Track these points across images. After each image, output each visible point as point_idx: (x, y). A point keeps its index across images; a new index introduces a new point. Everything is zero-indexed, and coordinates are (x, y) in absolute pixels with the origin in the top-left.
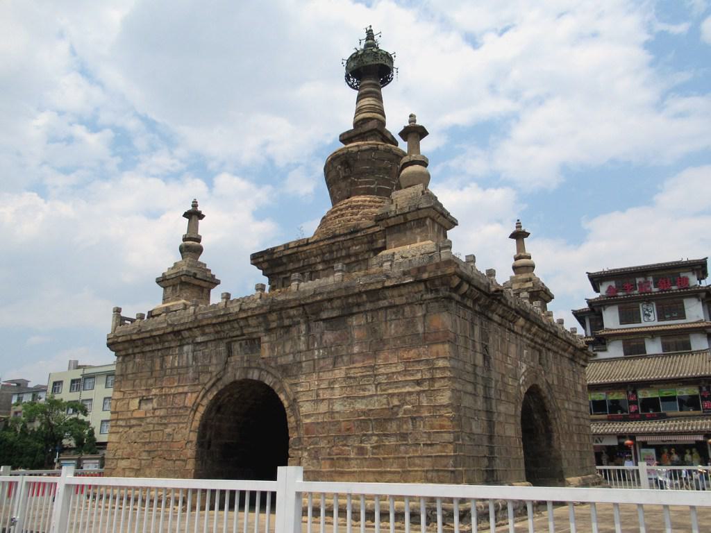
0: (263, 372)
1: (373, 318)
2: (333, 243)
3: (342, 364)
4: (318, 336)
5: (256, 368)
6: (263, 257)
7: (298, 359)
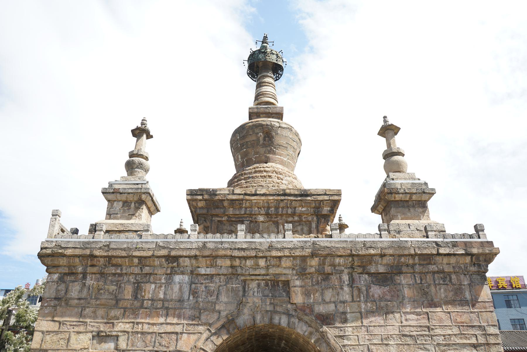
0: (292, 320)
1: (421, 280)
2: (282, 200)
3: (394, 321)
4: (364, 288)
5: (284, 313)
6: (202, 195)
7: (341, 310)
